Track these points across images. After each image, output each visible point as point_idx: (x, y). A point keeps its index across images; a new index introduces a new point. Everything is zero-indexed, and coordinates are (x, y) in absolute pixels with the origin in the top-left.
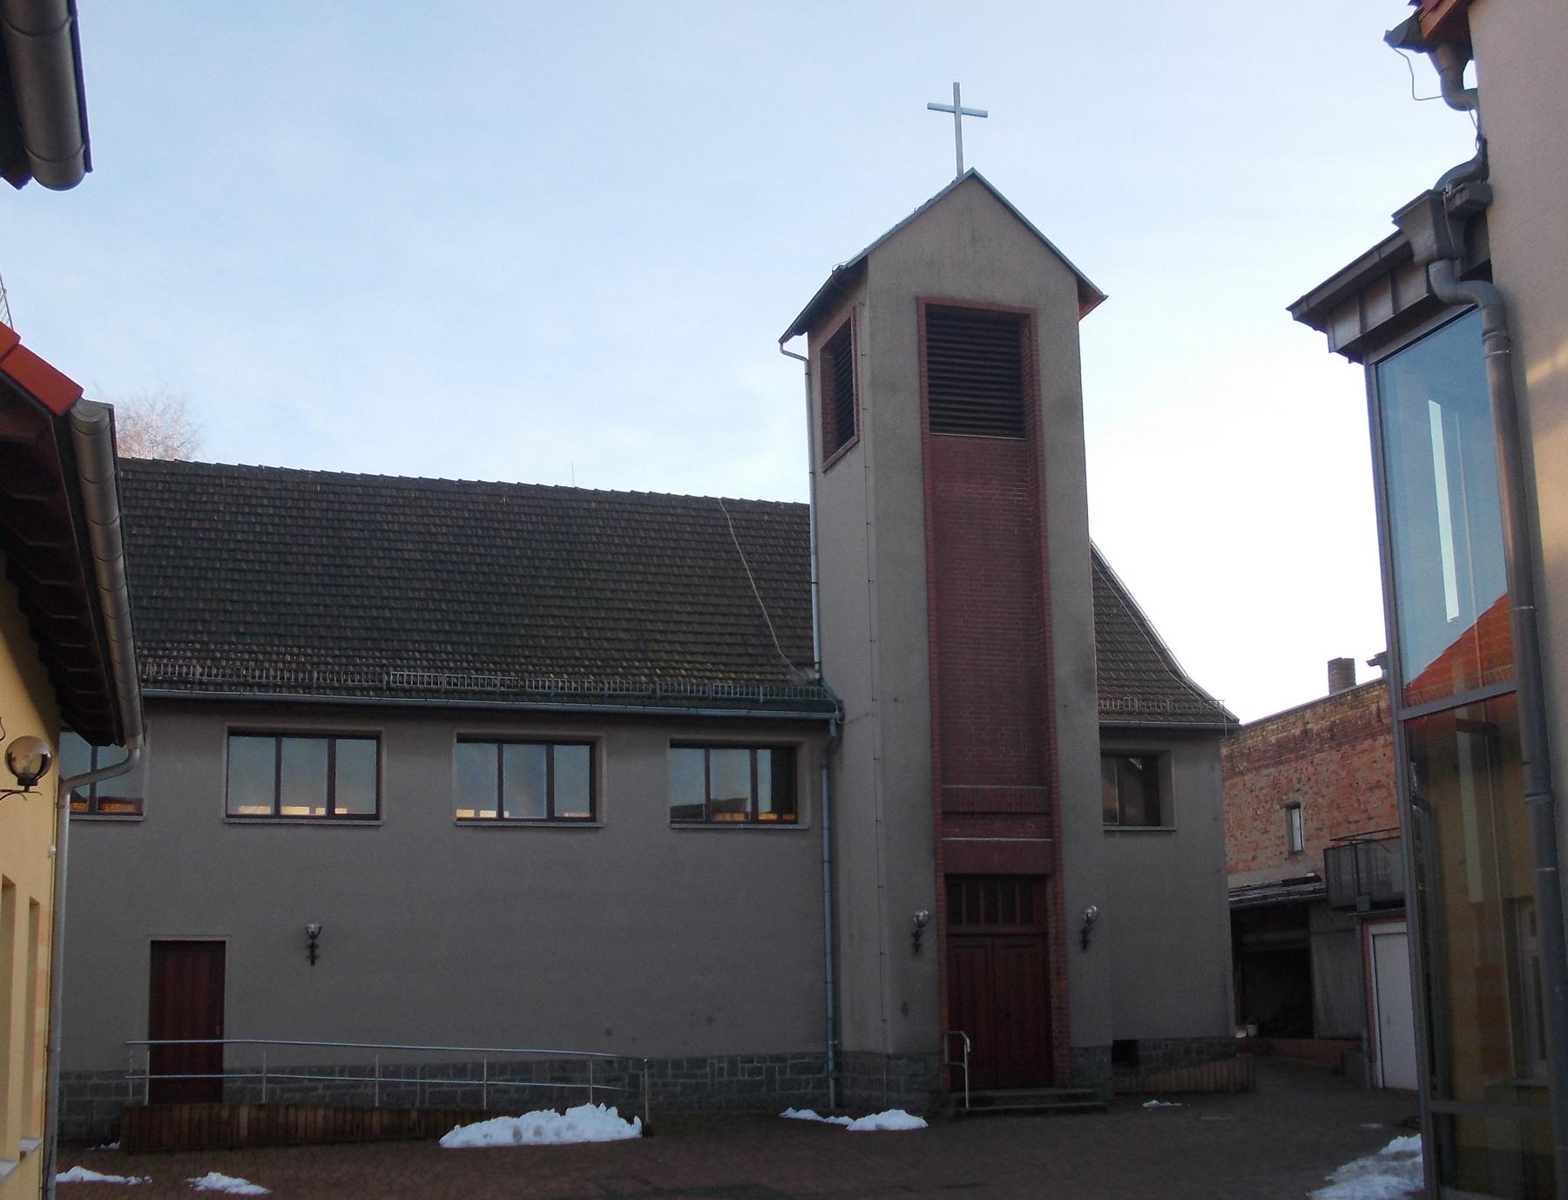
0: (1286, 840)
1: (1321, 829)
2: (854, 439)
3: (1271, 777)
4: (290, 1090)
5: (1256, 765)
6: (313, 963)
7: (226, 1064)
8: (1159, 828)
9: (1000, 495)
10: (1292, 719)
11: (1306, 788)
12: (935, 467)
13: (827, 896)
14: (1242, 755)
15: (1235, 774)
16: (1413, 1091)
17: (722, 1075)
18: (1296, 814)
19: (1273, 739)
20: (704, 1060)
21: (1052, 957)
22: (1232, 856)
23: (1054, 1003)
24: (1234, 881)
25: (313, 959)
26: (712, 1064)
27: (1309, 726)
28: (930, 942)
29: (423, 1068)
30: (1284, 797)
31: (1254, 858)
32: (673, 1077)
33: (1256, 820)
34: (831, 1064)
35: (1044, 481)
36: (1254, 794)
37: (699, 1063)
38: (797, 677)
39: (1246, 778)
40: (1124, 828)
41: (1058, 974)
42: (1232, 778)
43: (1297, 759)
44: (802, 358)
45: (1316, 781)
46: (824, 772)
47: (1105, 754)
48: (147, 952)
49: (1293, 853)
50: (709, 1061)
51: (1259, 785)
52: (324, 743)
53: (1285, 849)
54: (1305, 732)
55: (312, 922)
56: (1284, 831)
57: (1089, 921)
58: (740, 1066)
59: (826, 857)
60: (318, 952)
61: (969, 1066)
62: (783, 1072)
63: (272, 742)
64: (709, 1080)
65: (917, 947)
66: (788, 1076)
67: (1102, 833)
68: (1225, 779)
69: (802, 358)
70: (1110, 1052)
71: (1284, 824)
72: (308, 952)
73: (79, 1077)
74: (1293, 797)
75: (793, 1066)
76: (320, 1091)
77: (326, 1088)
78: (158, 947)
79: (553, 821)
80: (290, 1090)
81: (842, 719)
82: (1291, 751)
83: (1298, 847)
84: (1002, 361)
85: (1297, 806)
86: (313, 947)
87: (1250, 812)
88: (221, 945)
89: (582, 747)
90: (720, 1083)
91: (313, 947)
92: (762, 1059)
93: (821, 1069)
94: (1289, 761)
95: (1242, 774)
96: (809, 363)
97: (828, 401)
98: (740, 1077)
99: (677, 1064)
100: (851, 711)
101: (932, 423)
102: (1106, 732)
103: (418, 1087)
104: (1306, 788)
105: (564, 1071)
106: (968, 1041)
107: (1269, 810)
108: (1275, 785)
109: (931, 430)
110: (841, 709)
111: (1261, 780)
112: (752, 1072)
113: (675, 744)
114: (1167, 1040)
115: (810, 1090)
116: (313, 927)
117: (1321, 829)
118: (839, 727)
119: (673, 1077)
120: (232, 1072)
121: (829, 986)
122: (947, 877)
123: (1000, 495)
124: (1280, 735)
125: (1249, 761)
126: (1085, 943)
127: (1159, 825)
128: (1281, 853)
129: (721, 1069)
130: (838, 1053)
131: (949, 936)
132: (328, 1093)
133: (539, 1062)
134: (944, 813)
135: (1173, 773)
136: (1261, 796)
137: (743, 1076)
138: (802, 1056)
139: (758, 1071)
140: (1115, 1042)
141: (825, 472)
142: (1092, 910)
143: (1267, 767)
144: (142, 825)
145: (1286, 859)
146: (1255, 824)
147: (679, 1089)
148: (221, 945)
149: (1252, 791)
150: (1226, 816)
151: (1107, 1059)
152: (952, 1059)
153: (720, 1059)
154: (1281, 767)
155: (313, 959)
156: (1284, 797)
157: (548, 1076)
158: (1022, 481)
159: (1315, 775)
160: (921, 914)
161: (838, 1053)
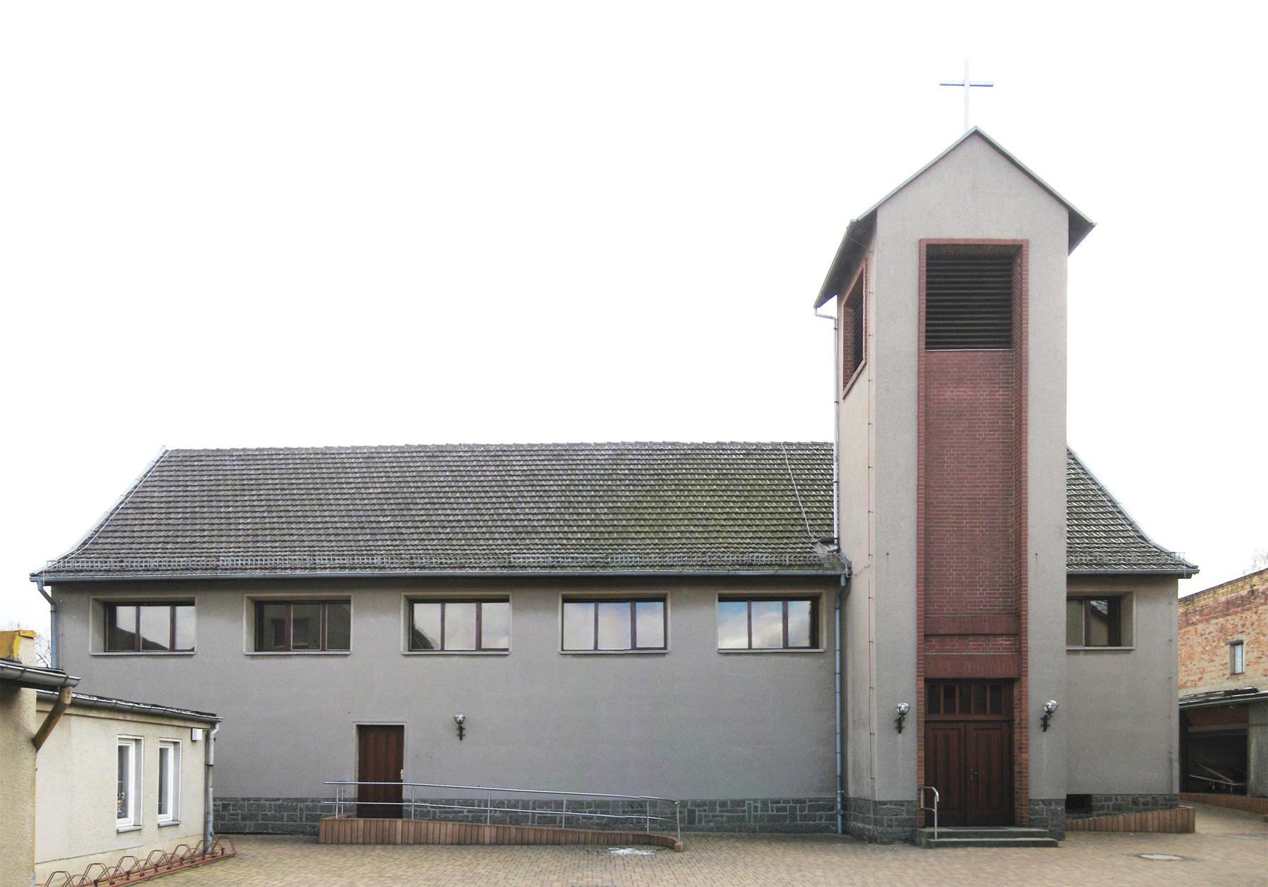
0: (1229, 666)
1: (1260, 658)
2: (863, 362)
3: (1220, 625)
4: (446, 812)
5: (1207, 617)
6: (461, 739)
7: (404, 796)
8: (1119, 648)
9: (987, 395)
10: (1240, 584)
11: (1250, 630)
12: (928, 378)
13: (838, 696)
14: (1196, 611)
15: (1189, 624)
16: (133, 634)
17: (757, 811)
18: (1238, 649)
19: (1223, 599)
20: (743, 801)
21: (1016, 737)
22: (1182, 678)
23: (1017, 768)
24: (1182, 694)
25: (461, 736)
26: (749, 804)
27: (1254, 588)
28: (911, 725)
29: (534, 803)
30: (1229, 638)
31: (1200, 679)
32: (720, 812)
33: (1204, 654)
34: (839, 806)
35: (1027, 380)
36: (1204, 637)
37: (740, 803)
38: (822, 551)
39: (1197, 626)
40: (1087, 648)
41: (1020, 748)
42: (1186, 627)
43: (1243, 611)
44: (831, 318)
45: (1259, 625)
46: (838, 612)
47: (1070, 598)
48: (354, 732)
49: (1234, 674)
50: (747, 802)
51: (1208, 631)
52: (473, 606)
53: (1228, 672)
54: (1252, 592)
55: (459, 713)
56: (1227, 660)
57: (1049, 712)
58: (770, 805)
59: (838, 671)
60: (464, 732)
61: (938, 810)
62: (802, 809)
63: (438, 606)
64: (746, 814)
65: (900, 728)
66: (806, 812)
67: (1065, 653)
68: (1181, 628)
69: (831, 318)
70: (1064, 803)
71: (1228, 656)
72: (458, 732)
73: (313, 801)
74: (1237, 637)
75: (810, 806)
76: (466, 813)
77: (441, 812)
78: (363, 730)
79: (637, 652)
80: (446, 812)
81: (850, 574)
82: (1239, 606)
83: (1239, 670)
84: (1000, 288)
85: (1240, 643)
86: (461, 729)
87: (1200, 649)
88: (400, 729)
89: (657, 603)
90: (754, 816)
91: (461, 729)
92: (787, 801)
93: (832, 808)
94: (1236, 613)
95: (1194, 624)
96: (837, 321)
97: (849, 344)
98: (770, 813)
99: (723, 804)
100: (855, 570)
101: (927, 343)
102: (1072, 578)
103: (530, 814)
104: (1250, 630)
105: (632, 807)
106: (937, 794)
107: (1215, 647)
108: (1222, 629)
109: (926, 348)
110: (850, 568)
111: (1213, 626)
112: (778, 810)
113: (722, 599)
114: (1117, 795)
115: (823, 821)
116: (460, 717)
117: (1260, 658)
118: (848, 580)
119: (720, 812)
120: (409, 801)
121: (838, 756)
122: (927, 681)
123: (987, 395)
124: (1229, 596)
125: (1201, 615)
126: (1045, 726)
127: (1120, 646)
128: (1224, 675)
129: (756, 807)
130: (845, 798)
131: (926, 722)
132: (470, 815)
133: (614, 802)
134: (925, 635)
135: (1134, 606)
136: (1210, 638)
137: (772, 811)
138: (819, 799)
139: (784, 809)
140: (1068, 796)
141: (844, 398)
142: (1051, 703)
143: (1217, 618)
144: (349, 657)
145: (1228, 679)
146: (1203, 656)
147: (725, 819)
148: (400, 729)
149: (1202, 635)
150: (1179, 652)
151: (1061, 808)
152: (926, 805)
153: (755, 801)
154: (1228, 618)
155: (461, 736)
156: (1229, 638)
157: (621, 810)
158: (1009, 383)
159: (1258, 621)
160: (903, 706)
161: (845, 798)
